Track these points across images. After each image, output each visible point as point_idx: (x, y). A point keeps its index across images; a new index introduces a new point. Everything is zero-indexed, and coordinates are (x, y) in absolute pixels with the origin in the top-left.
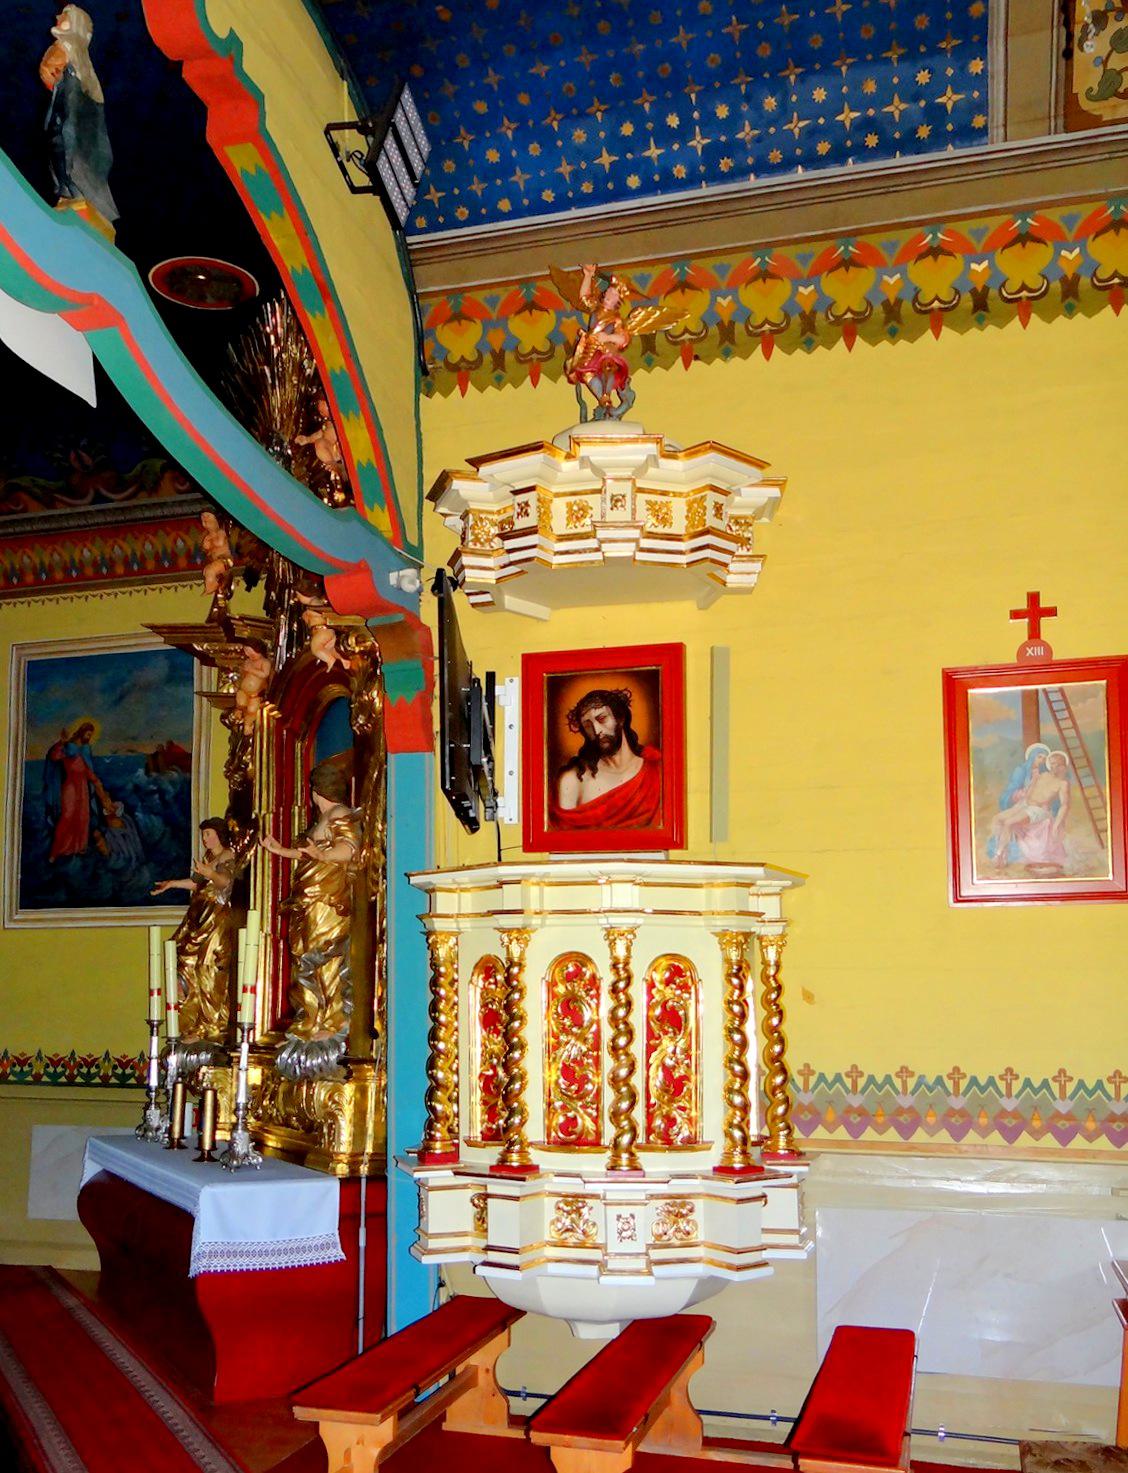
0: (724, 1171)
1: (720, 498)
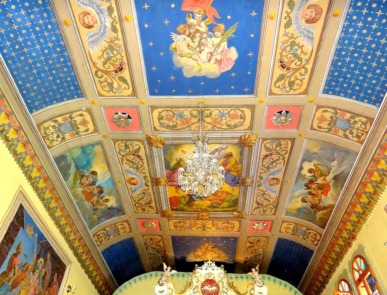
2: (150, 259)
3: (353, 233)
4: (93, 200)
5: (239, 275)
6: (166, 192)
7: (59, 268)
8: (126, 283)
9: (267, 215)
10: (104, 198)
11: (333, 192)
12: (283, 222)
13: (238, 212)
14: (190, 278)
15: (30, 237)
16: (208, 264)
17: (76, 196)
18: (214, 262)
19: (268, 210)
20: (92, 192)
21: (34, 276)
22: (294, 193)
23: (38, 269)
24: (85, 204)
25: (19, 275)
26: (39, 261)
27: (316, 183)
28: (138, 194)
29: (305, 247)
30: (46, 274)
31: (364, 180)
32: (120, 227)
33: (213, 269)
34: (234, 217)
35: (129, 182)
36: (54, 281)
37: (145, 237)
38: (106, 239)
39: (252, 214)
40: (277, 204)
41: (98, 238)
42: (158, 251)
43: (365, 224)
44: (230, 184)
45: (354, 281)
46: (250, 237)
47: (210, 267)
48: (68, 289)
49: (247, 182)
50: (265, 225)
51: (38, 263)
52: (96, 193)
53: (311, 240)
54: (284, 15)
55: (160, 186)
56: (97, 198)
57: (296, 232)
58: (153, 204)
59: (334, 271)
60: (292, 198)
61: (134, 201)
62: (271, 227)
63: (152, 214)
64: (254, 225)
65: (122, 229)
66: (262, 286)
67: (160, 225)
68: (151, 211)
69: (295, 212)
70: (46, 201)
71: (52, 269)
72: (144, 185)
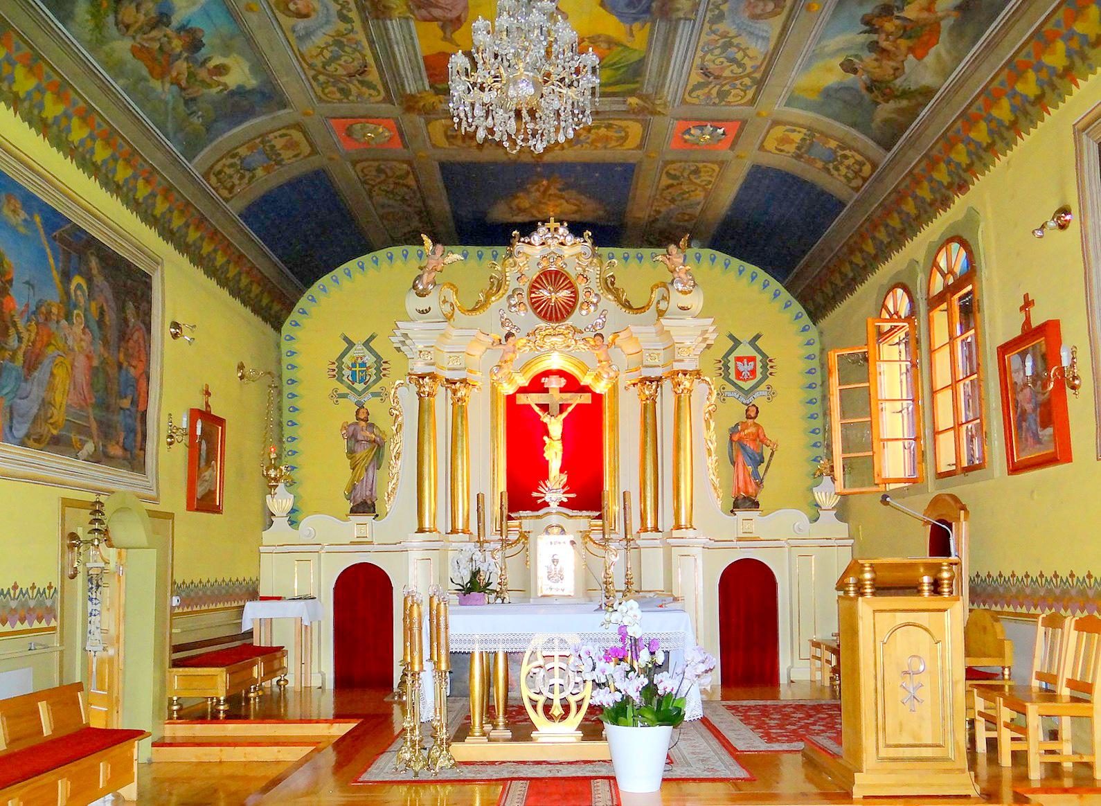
2: (382, 218)
3: (966, 176)
4: (174, 74)
5: (632, 252)
6: (412, 38)
7: (131, 286)
8: (326, 280)
9: (729, 104)
10: (212, 64)
11: (943, 53)
12: (776, 123)
13: (640, 97)
14: (499, 268)
15: (22, 230)
16: (549, 229)
17: (117, 69)
18: (566, 224)
19: (733, 92)
20: (167, 48)
21: (74, 328)
22: (824, 43)
23: (75, 306)
24: (153, 90)
25: (32, 339)
26: (72, 287)
27: (898, 18)
28: (319, 47)
29: (823, 193)
30: (102, 313)
31: (1048, 27)
32: (279, 143)
33: (562, 244)
34: (627, 112)
35: (282, 8)
36: (131, 325)
37: (359, 167)
38: (246, 180)
39: (684, 102)
40: (766, 74)
41: (219, 181)
42: (403, 200)
43: (1006, 155)
44: (621, 16)
45: (928, 294)
46: (673, 162)
47: (553, 238)
48: (173, 330)
49: (678, 10)
50: (720, 131)
51: (72, 291)
52: (178, 50)
53: (846, 176)
55: (389, 22)
56: (185, 65)
57: (806, 152)
58: (373, 76)
59: (886, 258)
60: (815, 56)
61: (311, 66)
62: (737, 137)
63: (373, 101)
64: (688, 131)
65: (286, 147)
66: (690, 292)
67: (402, 135)
68: (370, 95)
70: (26, 104)
71: (117, 296)
72: (335, 19)
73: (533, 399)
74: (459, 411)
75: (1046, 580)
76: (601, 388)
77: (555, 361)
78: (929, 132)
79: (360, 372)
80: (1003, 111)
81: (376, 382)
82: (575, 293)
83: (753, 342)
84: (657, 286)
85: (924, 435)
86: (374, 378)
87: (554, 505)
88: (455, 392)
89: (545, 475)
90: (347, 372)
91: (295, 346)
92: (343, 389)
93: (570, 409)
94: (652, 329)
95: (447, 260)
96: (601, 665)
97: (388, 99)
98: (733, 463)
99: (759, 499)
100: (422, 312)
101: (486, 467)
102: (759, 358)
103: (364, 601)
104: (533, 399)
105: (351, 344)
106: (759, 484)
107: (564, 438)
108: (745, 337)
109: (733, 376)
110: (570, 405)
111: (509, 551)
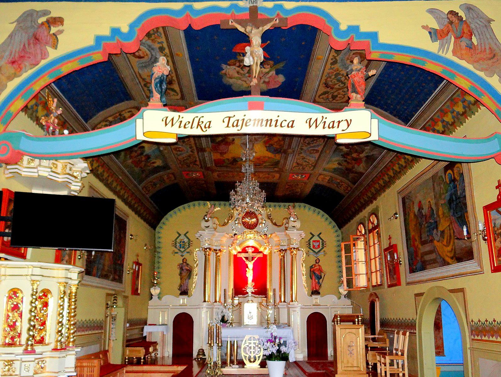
0: (55, 349)
1: (71, 166)
12: (320, 174)
17: (127, 167)
40: (316, 165)
54: (331, 57)
61: (180, 160)
69: (331, 170)
73: (243, 255)
74: (218, 260)
75: (482, 323)
76: (266, 252)
77: (251, 243)
78: (370, 177)
79: (184, 245)
80: (396, 168)
81: (188, 248)
82: (258, 220)
83: (318, 236)
84: (284, 219)
85: (369, 274)
86: (187, 247)
87: (250, 294)
88: (217, 254)
89: (246, 283)
90: (178, 245)
91: (160, 235)
92: (177, 251)
93: (255, 259)
94: (283, 233)
95: (215, 210)
96: (266, 343)
97: (201, 167)
98: (311, 279)
99: (320, 291)
100: (207, 227)
101: (226, 280)
102: (321, 241)
103: (183, 325)
104: (243, 255)
105: (180, 235)
106: (320, 286)
107: (254, 269)
108: (316, 234)
109: (312, 247)
110: (255, 257)
111: (234, 309)
